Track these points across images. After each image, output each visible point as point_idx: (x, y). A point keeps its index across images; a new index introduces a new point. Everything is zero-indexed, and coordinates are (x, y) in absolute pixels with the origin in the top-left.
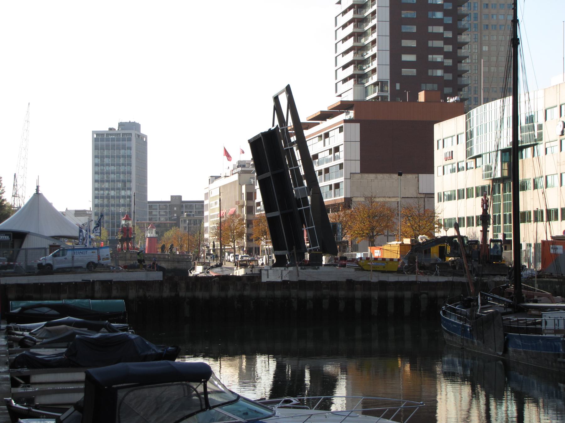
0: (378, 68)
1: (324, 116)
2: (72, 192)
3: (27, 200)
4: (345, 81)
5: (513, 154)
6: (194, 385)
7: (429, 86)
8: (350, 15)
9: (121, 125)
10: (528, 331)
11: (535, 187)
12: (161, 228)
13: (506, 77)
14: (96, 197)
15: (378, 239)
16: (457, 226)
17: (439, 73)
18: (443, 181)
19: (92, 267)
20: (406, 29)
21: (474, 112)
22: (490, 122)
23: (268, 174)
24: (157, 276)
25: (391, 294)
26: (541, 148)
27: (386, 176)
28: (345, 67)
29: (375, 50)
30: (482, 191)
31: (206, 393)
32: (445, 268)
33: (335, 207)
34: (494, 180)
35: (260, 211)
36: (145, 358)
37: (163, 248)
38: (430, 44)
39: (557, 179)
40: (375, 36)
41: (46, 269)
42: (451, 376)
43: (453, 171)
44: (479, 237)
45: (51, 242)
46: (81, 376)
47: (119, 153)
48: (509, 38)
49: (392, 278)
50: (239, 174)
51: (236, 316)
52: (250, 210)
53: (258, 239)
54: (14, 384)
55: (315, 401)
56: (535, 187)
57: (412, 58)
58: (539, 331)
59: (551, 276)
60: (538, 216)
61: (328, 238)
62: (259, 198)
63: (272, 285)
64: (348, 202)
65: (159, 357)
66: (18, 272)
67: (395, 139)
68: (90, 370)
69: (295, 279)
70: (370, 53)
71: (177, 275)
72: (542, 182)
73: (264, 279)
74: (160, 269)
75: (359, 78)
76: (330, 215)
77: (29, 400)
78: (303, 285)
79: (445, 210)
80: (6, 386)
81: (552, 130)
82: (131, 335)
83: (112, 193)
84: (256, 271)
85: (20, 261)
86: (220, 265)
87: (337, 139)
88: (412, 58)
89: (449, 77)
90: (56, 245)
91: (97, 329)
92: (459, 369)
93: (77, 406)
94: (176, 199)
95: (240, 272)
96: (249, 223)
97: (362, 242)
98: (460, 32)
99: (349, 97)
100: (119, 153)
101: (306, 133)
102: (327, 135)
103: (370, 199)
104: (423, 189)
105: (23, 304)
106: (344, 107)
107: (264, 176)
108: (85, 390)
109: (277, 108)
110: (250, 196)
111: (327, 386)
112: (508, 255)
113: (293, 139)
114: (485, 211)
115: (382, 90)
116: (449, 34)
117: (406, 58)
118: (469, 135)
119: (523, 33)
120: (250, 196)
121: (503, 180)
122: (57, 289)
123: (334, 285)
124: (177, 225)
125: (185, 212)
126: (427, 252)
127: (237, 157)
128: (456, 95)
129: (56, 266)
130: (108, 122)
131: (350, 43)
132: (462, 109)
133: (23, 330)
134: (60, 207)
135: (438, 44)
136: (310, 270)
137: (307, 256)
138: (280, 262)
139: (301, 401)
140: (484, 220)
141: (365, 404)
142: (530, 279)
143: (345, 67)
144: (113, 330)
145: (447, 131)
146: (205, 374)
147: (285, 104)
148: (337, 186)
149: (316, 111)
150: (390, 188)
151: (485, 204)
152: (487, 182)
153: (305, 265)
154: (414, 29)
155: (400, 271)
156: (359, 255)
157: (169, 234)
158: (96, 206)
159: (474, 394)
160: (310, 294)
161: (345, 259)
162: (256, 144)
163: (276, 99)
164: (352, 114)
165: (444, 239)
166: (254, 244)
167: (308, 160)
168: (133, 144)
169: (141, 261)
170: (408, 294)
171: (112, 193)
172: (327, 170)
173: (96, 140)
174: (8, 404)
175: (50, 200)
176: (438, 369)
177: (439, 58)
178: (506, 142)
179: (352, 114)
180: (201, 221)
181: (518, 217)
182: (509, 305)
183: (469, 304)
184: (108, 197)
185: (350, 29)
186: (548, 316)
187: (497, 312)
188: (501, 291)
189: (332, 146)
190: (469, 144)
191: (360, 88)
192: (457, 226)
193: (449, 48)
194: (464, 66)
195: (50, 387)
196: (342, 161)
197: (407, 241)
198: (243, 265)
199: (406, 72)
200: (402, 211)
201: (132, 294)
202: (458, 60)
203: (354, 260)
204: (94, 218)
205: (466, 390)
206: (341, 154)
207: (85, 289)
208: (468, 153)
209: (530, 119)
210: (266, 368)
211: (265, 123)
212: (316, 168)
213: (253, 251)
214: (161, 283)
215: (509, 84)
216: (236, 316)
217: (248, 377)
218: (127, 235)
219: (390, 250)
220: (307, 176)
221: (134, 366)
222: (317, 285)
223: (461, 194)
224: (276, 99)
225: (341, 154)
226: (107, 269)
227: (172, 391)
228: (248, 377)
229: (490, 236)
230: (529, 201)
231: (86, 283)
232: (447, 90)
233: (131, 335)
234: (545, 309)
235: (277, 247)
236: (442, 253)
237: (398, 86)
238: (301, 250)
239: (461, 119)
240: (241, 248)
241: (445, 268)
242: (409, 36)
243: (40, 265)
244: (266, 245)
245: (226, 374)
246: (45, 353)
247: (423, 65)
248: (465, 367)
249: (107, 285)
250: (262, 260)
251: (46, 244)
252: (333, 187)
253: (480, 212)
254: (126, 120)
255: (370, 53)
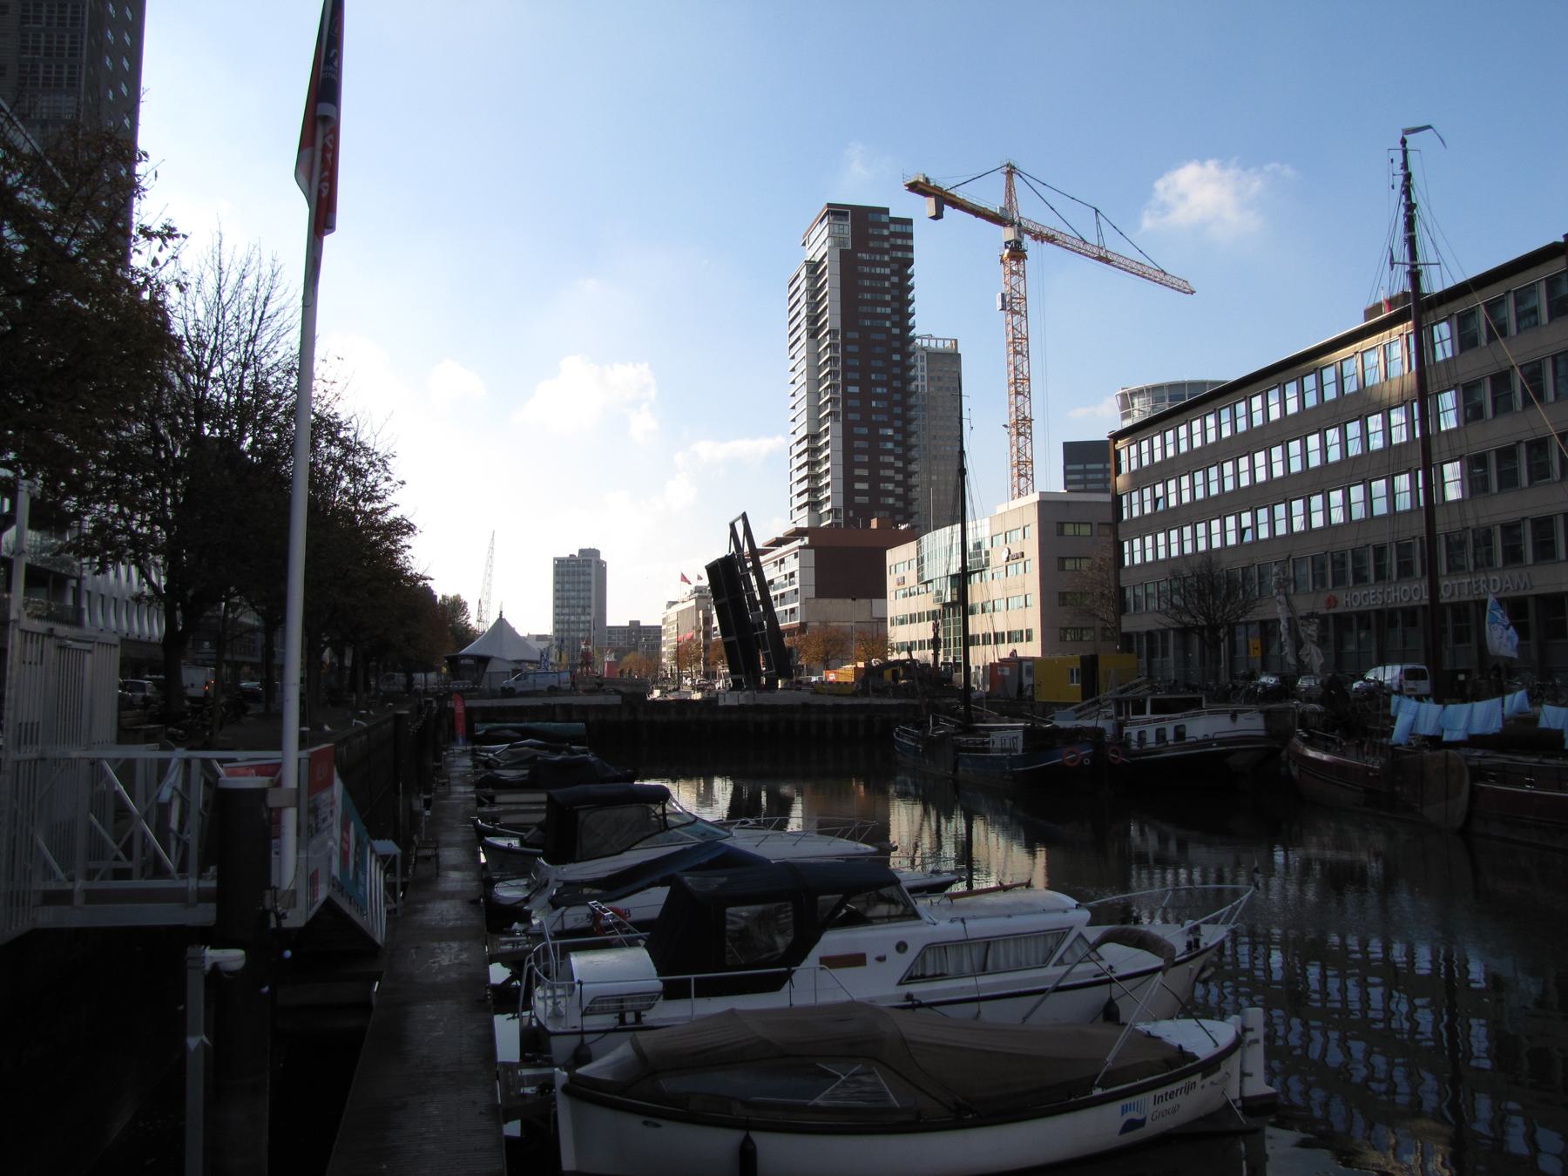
0: (830, 497)
1: (779, 542)
2: (533, 616)
3: (491, 625)
4: (799, 508)
5: (961, 580)
6: (653, 807)
7: (882, 514)
8: (804, 445)
9: (581, 551)
10: (977, 750)
11: (983, 611)
12: (620, 653)
13: (955, 506)
14: (556, 622)
15: (832, 663)
16: (909, 650)
17: (891, 501)
18: (896, 605)
19: (553, 690)
20: (859, 458)
21: (924, 538)
22: (941, 547)
23: (725, 600)
24: (617, 700)
25: (846, 716)
26: (988, 573)
27: (840, 601)
28: (799, 495)
29: (828, 465)
30: (933, 615)
31: (664, 814)
32: (899, 691)
33: (791, 631)
34: (945, 605)
35: (717, 636)
36: (603, 782)
37: (622, 672)
38: (882, 473)
39: (1003, 603)
40: (828, 465)
41: (508, 693)
42: (903, 795)
43: (905, 596)
44: (931, 660)
45: (514, 666)
46: (543, 797)
47: (579, 578)
48: (956, 468)
49: (846, 701)
50: (697, 599)
51: (694, 740)
52: (707, 635)
53: (715, 663)
54: (480, 803)
55: (771, 822)
56: (983, 611)
57: (864, 486)
58: (987, 750)
59: (998, 697)
60: (986, 639)
61: (784, 663)
62: (716, 623)
63: (728, 709)
64: (803, 627)
65: (617, 779)
66: (482, 695)
67: (847, 563)
68: (552, 792)
69: (751, 702)
70: (824, 481)
71: (635, 698)
72: (990, 606)
73: (721, 703)
74: (618, 692)
75: (814, 505)
76: (786, 639)
77: (493, 819)
78: (758, 708)
79: (898, 634)
80: (472, 805)
81: (998, 557)
82: (591, 757)
83: (573, 618)
84: (713, 695)
85: (484, 686)
86: (677, 690)
87: (793, 565)
88: (864, 486)
89: (900, 504)
90: (518, 668)
91: (558, 751)
92: (912, 789)
93: (539, 826)
94: (635, 624)
95: (697, 696)
96: (706, 648)
97: (815, 665)
98: (910, 461)
99: (804, 524)
100: (579, 578)
101: (762, 559)
102: (782, 561)
103: (825, 624)
104: (877, 614)
105: (488, 726)
106: (798, 533)
107: (729, 639)
108: (547, 811)
109: (734, 534)
110: (708, 621)
111: (782, 807)
112: (959, 677)
113: (749, 565)
114: (936, 635)
115: (836, 517)
116: (900, 464)
117: (858, 486)
118: (920, 561)
119: (969, 463)
120: (708, 621)
121: (953, 604)
122: (519, 712)
123: (790, 708)
124: (636, 649)
125: (642, 637)
126: (881, 675)
127: (695, 583)
128: (909, 521)
129: (518, 690)
130: (570, 549)
131: (805, 471)
132: (913, 535)
133: (488, 751)
134: (522, 631)
135: (890, 473)
136: (766, 694)
137: (764, 680)
138: (737, 686)
139: (758, 822)
140: (935, 643)
141: (820, 825)
142: (979, 701)
143: (799, 495)
144: (573, 752)
145: (899, 559)
146: (664, 796)
147: (741, 530)
148: (793, 611)
149: (771, 537)
150: (844, 613)
151: (936, 627)
152: (938, 607)
153: (761, 689)
154: (865, 472)
155: (854, 695)
156: (814, 679)
157: (628, 658)
158: (556, 630)
159: (926, 812)
160: (766, 717)
161: (800, 682)
162: (712, 569)
163: (732, 526)
164: (806, 540)
165: (897, 662)
166: (711, 668)
167: (764, 586)
168: (593, 570)
169: (600, 686)
170: (862, 717)
171: (573, 618)
172: (782, 595)
173: (556, 567)
174: (475, 823)
175: (513, 625)
176: (892, 791)
177: (890, 487)
178: (955, 568)
179: (806, 540)
180: (659, 646)
181: (968, 641)
182: (959, 726)
183: (922, 725)
184: (568, 622)
185: (804, 458)
186: (995, 736)
187: (946, 734)
188: (952, 713)
189: (788, 572)
190: (920, 569)
191: (814, 514)
192: (909, 650)
193: (900, 477)
194: (914, 494)
195: (514, 808)
196: (797, 586)
197: (861, 665)
198: (699, 688)
199: (858, 499)
200: (855, 635)
201: (592, 718)
202: (909, 488)
203: (809, 684)
204: (555, 643)
205: (918, 809)
206: (797, 579)
207: (547, 712)
208: (920, 578)
209: (978, 546)
210: (723, 790)
211: (722, 549)
212: (772, 594)
213: (710, 675)
214: (619, 707)
215: (958, 514)
216: (694, 740)
217: (706, 799)
218: (587, 659)
219: (845, 673)
220: (762, 601)
221: (594, 788)
222: (773, 708)
223: (912, 619)
224: (732, 526)
225: (797, 579)
226: (568, 692)
227: (632, 812)
228: (706, 799)
229: (941, 659)
230: (977, 625)
231: (547, 707)
232: (898, 517)
233: (591, 757)
234: (992, 729)
235: (733, 672)
236: (895, 676)
237: (851, 514)
238: (759, 673)
239: (913, 545)
240: (698, 672)
241: (899, 691)
242: (861, 465)
243: (503, 689)
244: (723, 669)
245: (683, 796)
246: (509, 774)
247: (875, 492)
248: (916, 786)
249: (567, 708)
250: (719, 684)
251: (509, 668)
252: (788, 613)
253: (931, 636)
254: (586, 547)
255: (824, 481)
